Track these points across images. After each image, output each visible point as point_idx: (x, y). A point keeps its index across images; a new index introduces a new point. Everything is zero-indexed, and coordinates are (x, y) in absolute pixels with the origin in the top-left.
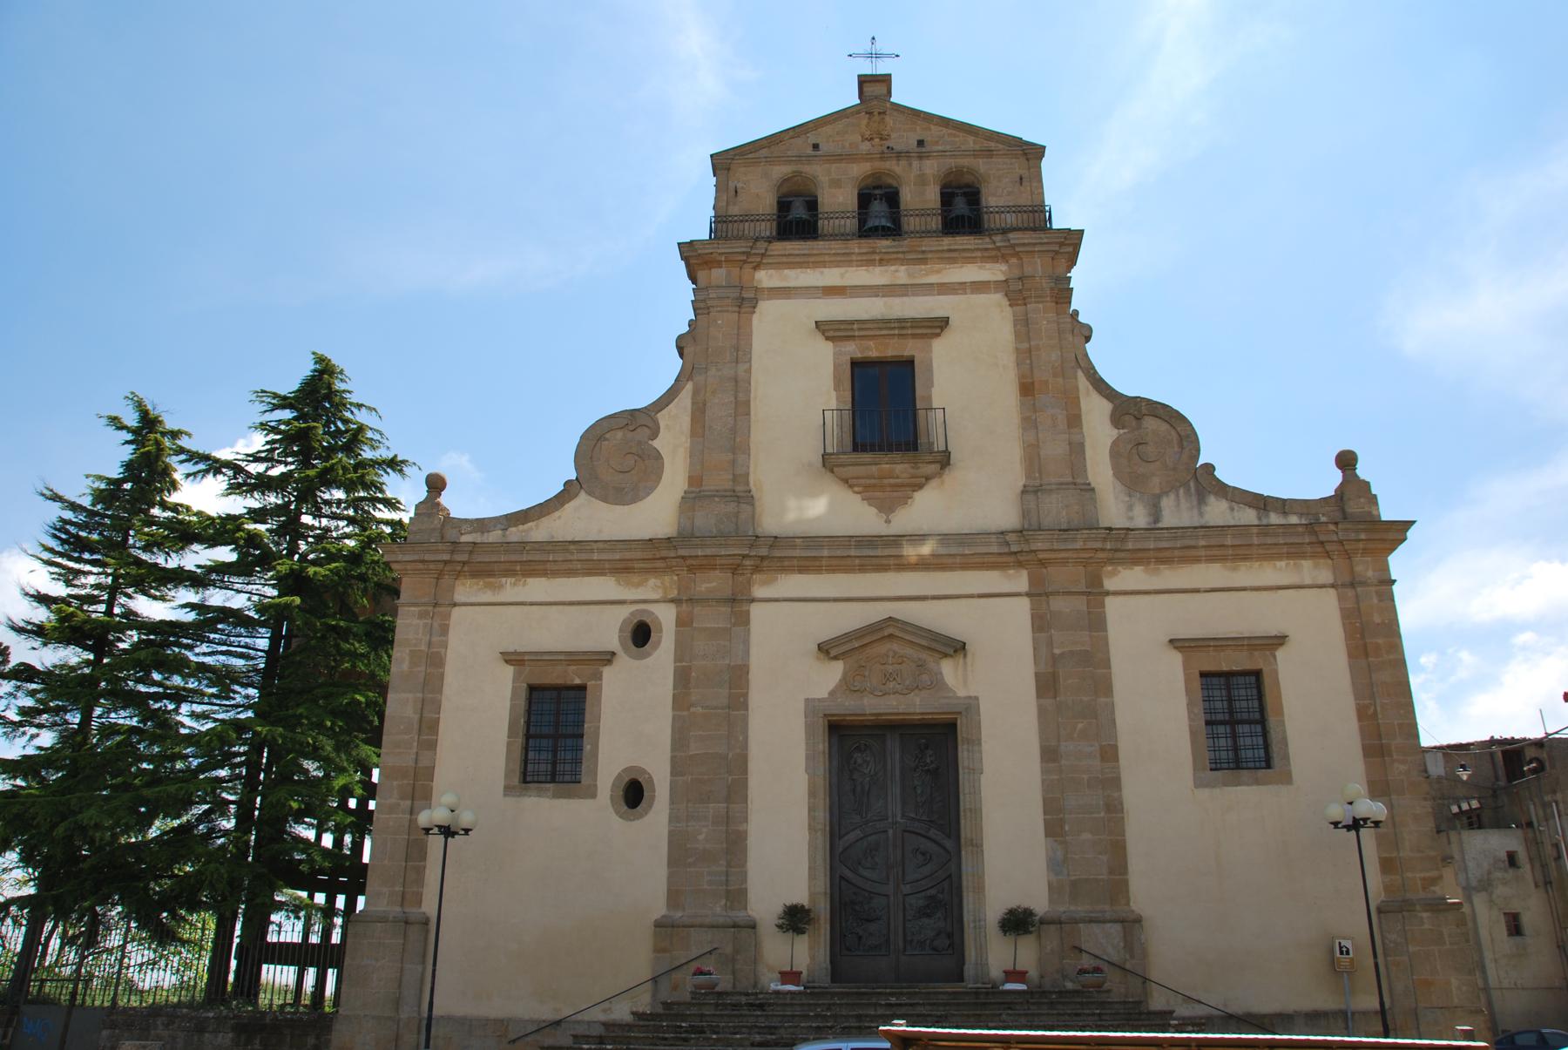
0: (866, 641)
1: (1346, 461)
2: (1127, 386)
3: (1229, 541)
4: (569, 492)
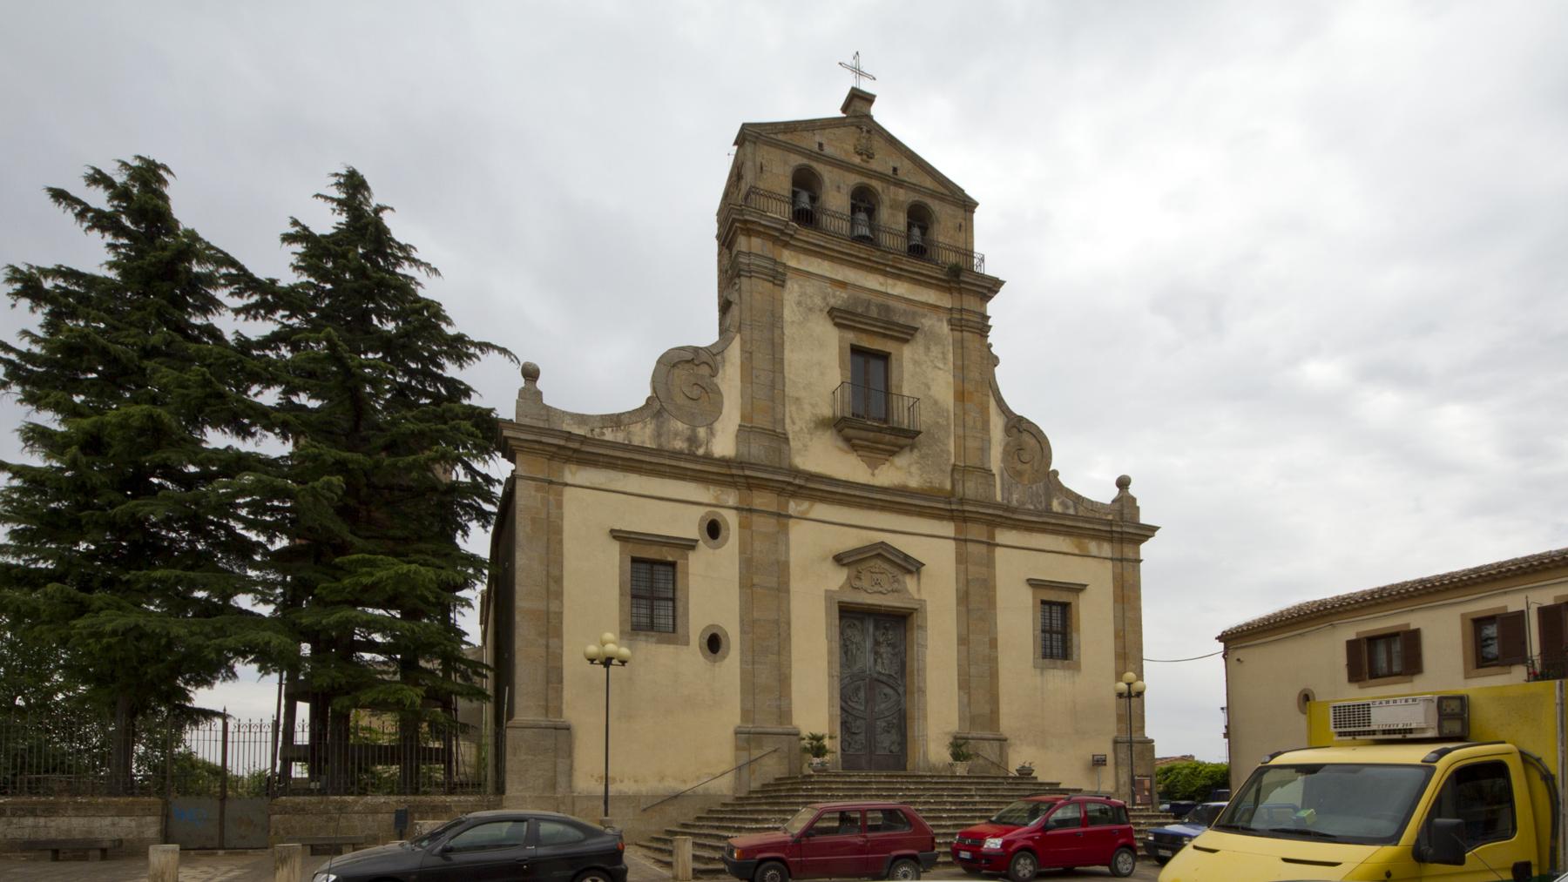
1: (1123, 483)
2: (1017, 408)
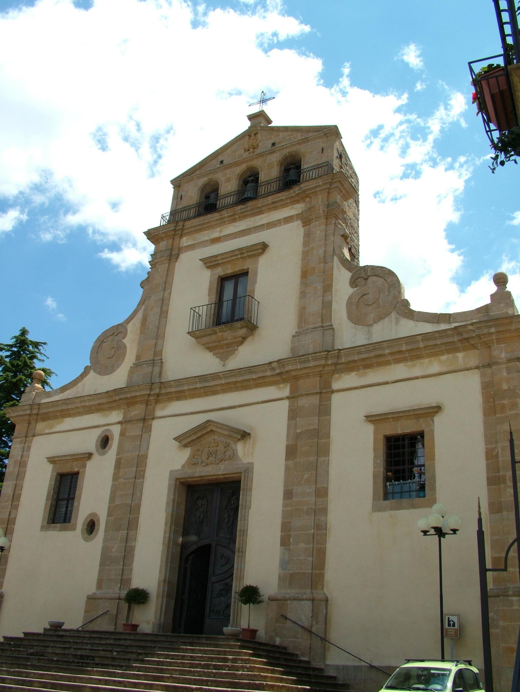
0: (199, 435)
3: (404, 348)
4: (87, 370)
